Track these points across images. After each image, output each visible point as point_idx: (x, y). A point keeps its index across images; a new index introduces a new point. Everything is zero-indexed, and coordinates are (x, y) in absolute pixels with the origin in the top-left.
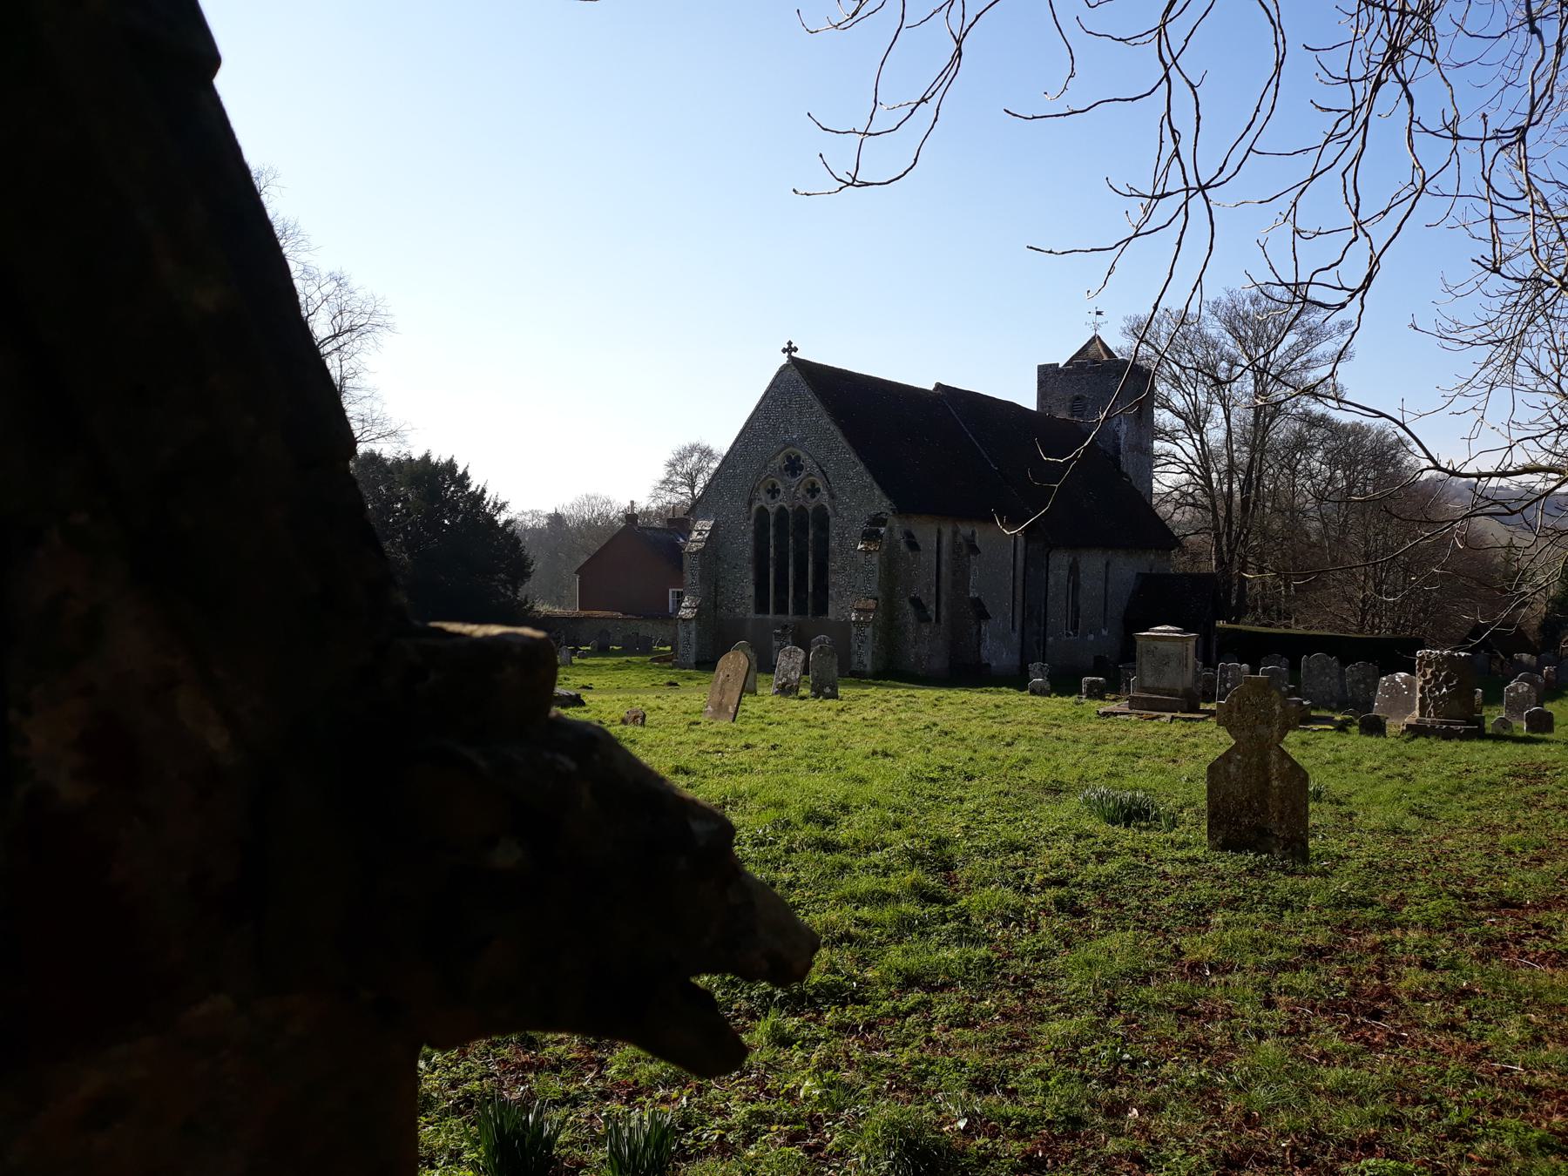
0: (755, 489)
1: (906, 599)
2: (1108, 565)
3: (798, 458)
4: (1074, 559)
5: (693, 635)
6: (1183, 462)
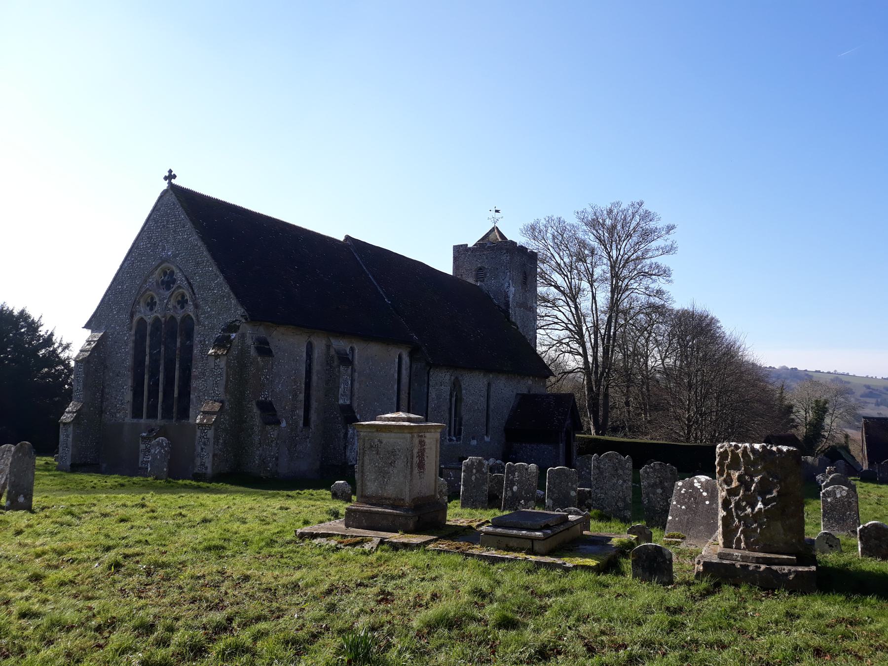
0: (136, 303)
1: (254, 403)
2: (489, 385)
3: (172, 273)
4: (457, 378)
5: (70, 439)
6: (563, 322)
